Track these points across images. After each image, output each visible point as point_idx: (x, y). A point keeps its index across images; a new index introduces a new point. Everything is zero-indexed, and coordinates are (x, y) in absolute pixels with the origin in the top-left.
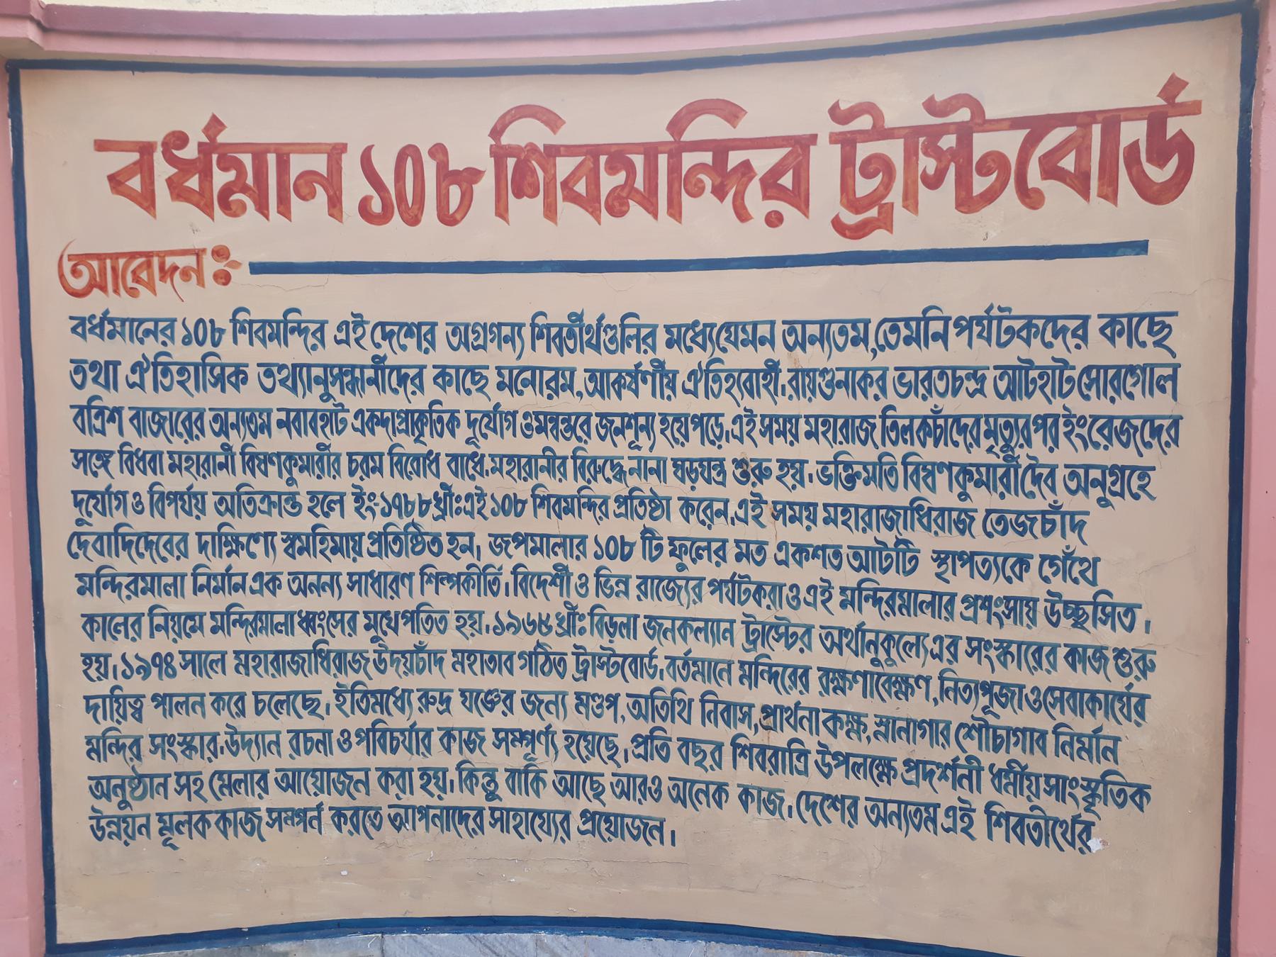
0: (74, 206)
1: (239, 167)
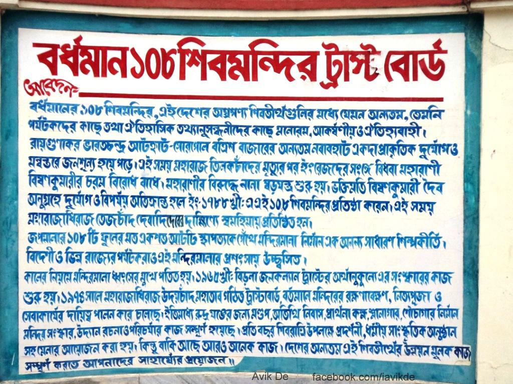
0: (29, 66)
1: (89, 55)
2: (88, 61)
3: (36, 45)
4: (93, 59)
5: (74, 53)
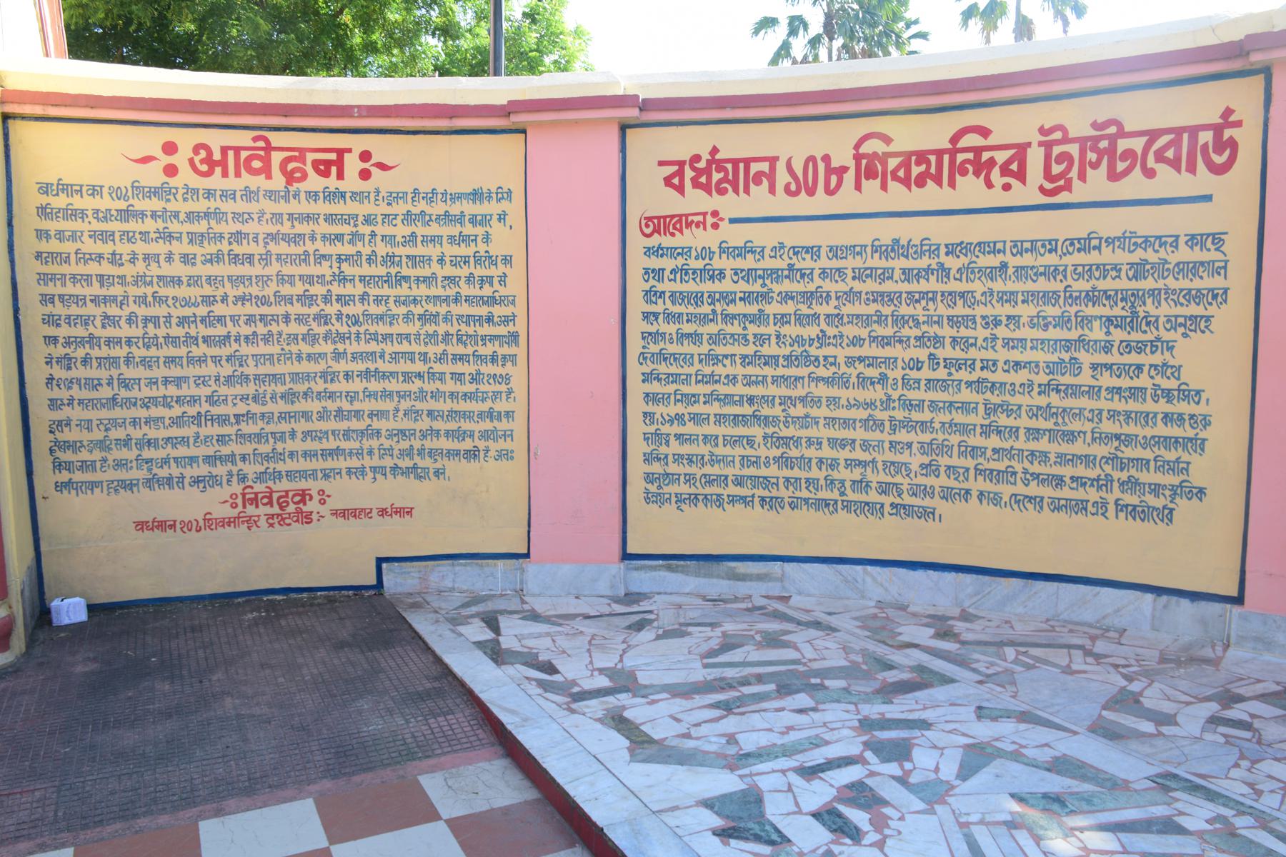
2: (725, 180)
3: (661, 163)
4: (730, 177)
5: (707, 171)
